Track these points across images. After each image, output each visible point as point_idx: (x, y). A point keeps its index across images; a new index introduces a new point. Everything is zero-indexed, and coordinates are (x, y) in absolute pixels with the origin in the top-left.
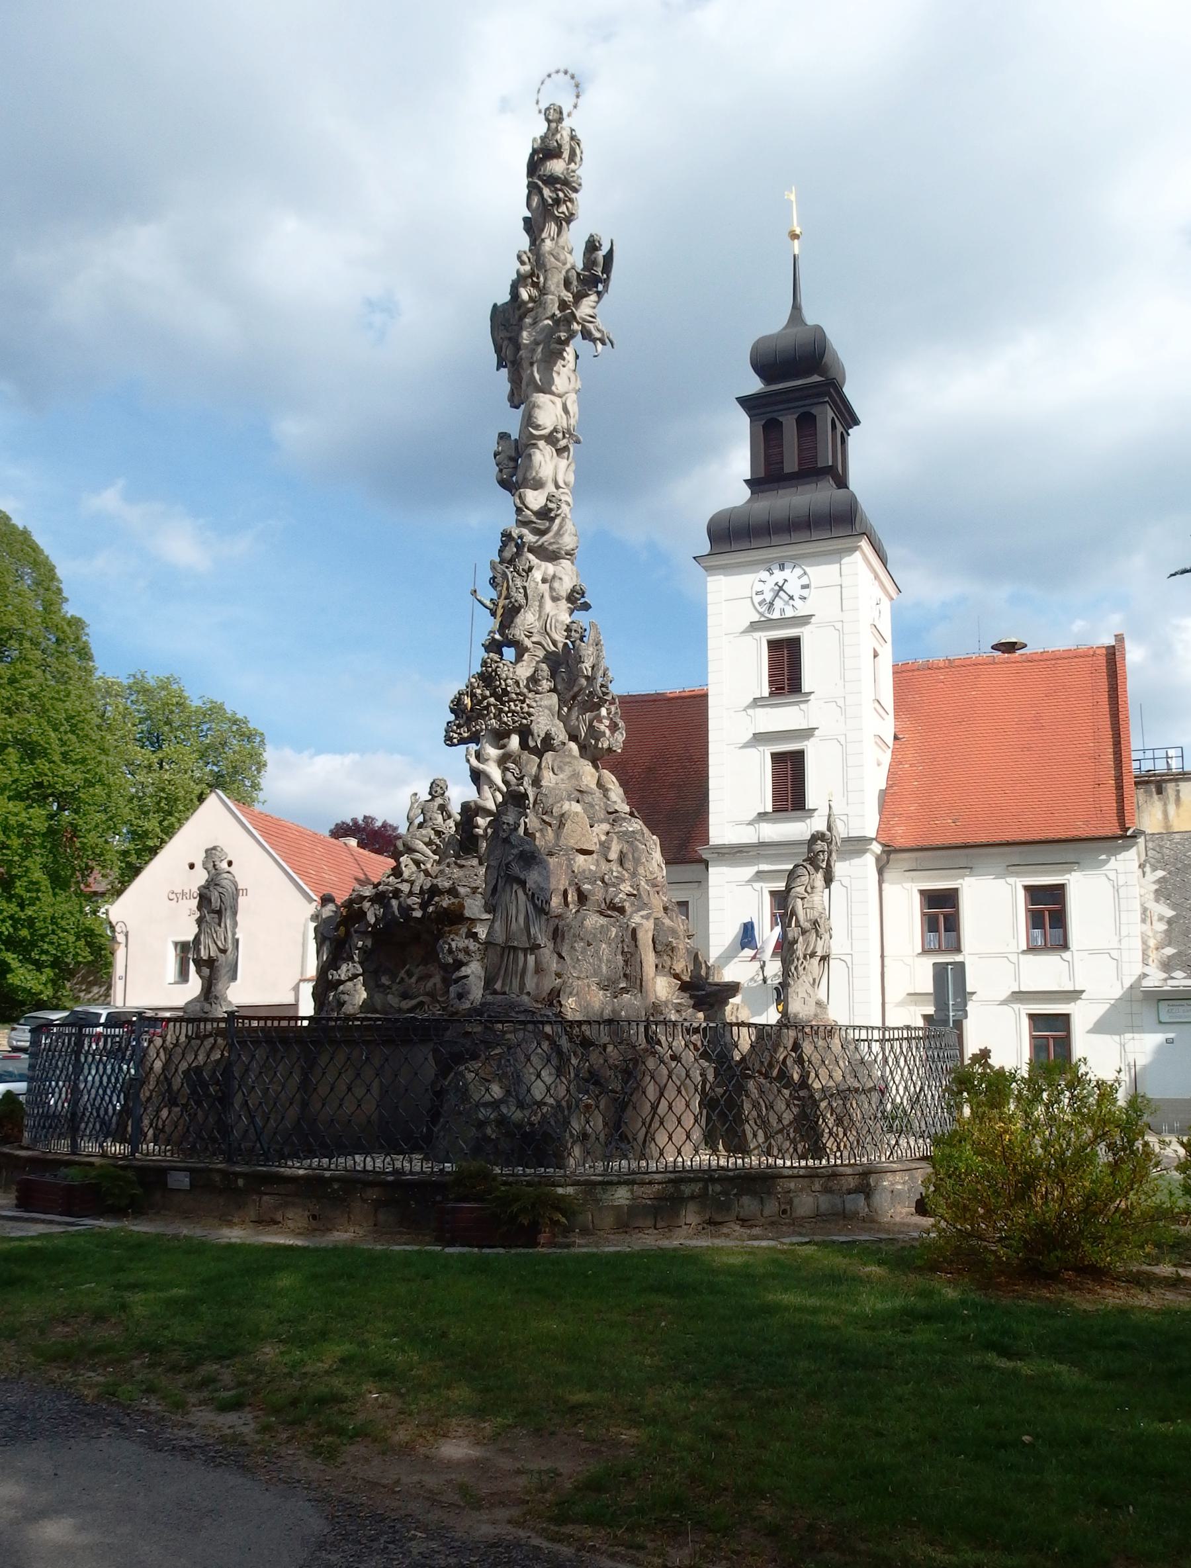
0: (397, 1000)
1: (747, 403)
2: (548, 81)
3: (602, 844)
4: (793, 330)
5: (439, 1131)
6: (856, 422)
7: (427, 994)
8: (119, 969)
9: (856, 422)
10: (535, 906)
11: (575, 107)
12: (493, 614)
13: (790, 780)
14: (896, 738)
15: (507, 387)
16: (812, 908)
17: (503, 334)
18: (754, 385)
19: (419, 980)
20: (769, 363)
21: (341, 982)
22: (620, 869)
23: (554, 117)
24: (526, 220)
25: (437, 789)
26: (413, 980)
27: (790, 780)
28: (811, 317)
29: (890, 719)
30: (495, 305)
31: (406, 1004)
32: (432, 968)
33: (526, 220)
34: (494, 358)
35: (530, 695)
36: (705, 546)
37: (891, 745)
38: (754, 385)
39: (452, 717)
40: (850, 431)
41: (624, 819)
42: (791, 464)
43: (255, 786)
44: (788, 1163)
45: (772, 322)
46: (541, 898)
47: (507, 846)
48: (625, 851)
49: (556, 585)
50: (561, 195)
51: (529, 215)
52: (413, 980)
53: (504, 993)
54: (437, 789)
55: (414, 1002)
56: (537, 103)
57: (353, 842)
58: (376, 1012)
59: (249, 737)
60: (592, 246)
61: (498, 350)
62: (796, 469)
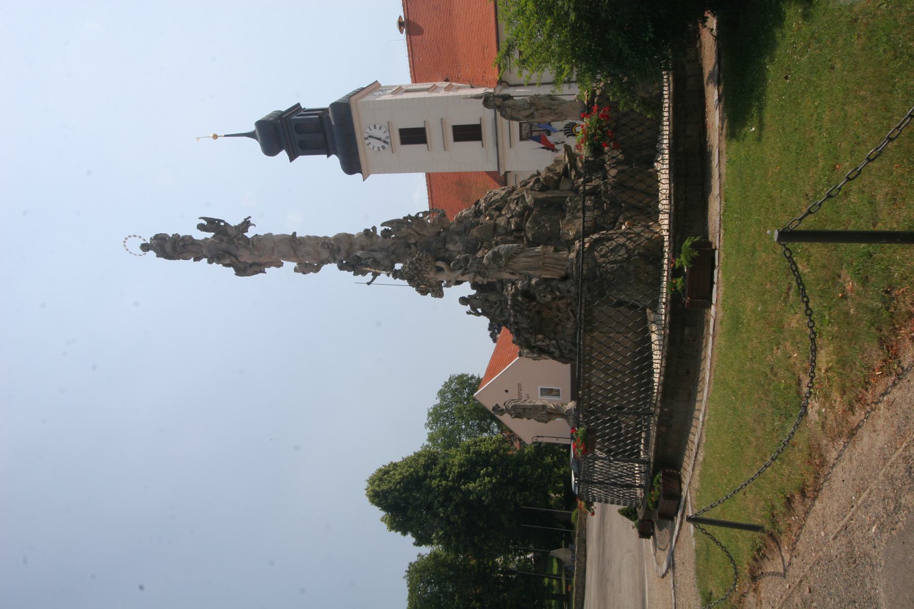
1: (292, 158)
6: (299, 104)
8: (554, 441)
9: (299, 104)
12: (379, 274)
14: (447, 80)
15: (273, 268)
18: (283, 154)
19: (559, 311)
20: (270, 150)
21: (550, 37)
23: (145, 247)
24: (195, 260)
25: (464, 301)
27: (467, 133)
31: (573, 319)
33: (195, 260)
34: (260, 274)
36: (358, 176)
38: (283, 154)
39: (429, 294)
43: (473, 377)
45: (255, 145)
54: (464, 301)
55: (571, 314)
57: (498, 336)
58: (575, 333)
59: (451, 381)
60: (201, 227)
61: (256, 273)
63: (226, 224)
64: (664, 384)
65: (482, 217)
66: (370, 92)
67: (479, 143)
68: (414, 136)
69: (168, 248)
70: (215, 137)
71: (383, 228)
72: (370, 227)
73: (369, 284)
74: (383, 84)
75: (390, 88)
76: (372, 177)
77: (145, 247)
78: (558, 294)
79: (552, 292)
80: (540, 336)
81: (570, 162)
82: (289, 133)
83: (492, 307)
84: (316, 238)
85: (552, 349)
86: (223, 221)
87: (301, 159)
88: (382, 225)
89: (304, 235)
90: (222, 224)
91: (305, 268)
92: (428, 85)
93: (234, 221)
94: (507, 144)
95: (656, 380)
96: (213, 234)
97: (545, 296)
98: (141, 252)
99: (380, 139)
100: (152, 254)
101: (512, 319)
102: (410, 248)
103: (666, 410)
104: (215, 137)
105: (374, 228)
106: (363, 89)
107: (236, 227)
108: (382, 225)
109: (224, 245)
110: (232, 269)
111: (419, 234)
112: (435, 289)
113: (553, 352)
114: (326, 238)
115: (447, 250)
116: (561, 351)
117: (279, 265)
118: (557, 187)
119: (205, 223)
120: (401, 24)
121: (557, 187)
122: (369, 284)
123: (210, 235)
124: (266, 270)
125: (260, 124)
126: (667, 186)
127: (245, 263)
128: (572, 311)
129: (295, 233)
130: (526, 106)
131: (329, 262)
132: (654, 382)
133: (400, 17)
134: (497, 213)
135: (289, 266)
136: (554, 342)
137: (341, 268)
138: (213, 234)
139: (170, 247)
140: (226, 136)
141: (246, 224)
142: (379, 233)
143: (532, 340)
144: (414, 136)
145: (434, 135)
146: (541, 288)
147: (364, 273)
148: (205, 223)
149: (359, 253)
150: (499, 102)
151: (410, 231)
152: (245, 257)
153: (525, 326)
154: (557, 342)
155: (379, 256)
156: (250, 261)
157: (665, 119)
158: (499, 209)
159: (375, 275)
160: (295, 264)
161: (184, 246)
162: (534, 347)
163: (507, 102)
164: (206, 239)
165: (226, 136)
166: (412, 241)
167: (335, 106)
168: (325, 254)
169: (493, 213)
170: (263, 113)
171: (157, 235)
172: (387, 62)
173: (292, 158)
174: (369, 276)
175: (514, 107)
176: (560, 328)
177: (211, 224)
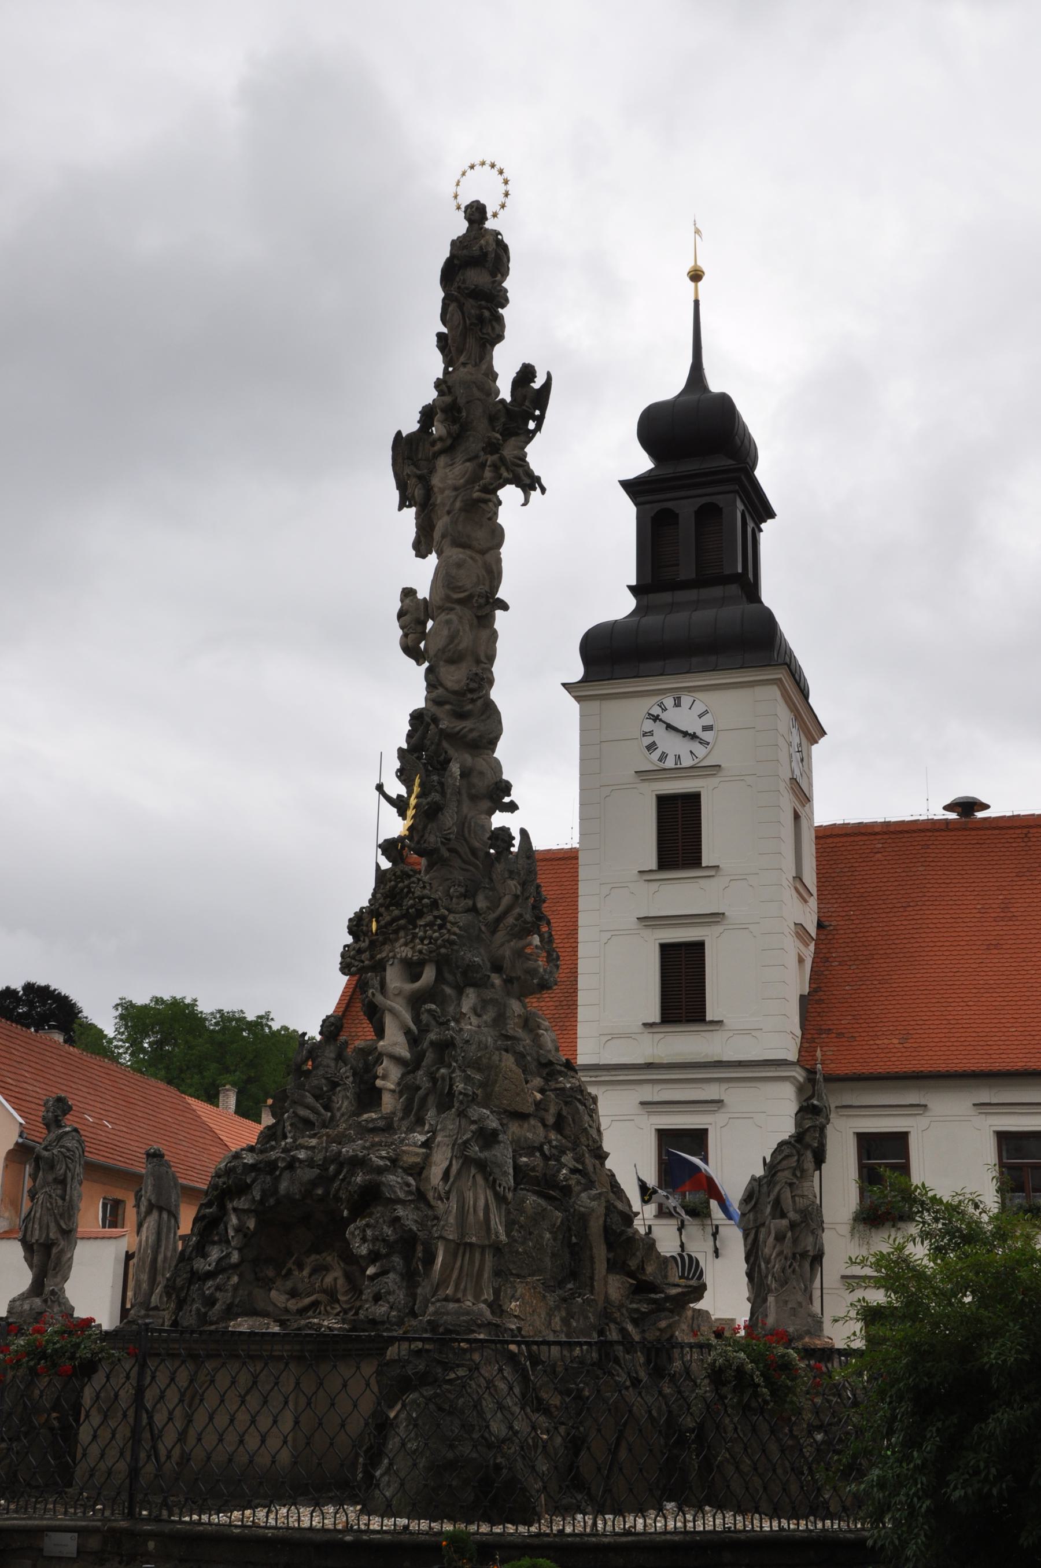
0: (283, 1298)
1: (631, 487)
2: (469, 172)
3: (537, 1104)
4: (693, 397)
5: (382, 1475)
6: (770, 514)
7: (324, 1291)
9: (770, 514)
10: (496, 1195)
11: (503, 206)
12: (402, 814)
13: (683, 984)
14: (820, 926)
16: (803, 1196)
17: (408, 470)
18: (641, 463)
20: (658, 428)
22: (559, 1137)
23: (476, 213)
24: (440, 336)
26: (306, 1273)
27: (683, 984)
28: (715, 384)
29: (813, 902)
30: (399, 433)
31: (293, 1305)
32: (329, 1258)
33: (440, 336)
34: (396, 495)
35: (451, 918)
36: (576, 671)
37: (814, 935)
38: (641, 463)
39: (349, 940)
40: (763, 526)
41: (560, 1073)
42: (687, 571)
44: (671, 1525)
45: (670, 385)
46: (504, 1184)
47: (463, 1121)
48: (564, 1113)
49: (475, 780)
50: (486, 313)
51: (445, 330)
52: (306, 1273)
53: (458, 1301)
55: (307, 1301)
56: (456, 197)
60: (527, 373)
62: (694, 576)
63: (530, 435)
64: (221, 1538)
65: (538, 1081)
66: (798, 717)
67: (655, 1016)
68: (680, 834)
69: (476, 277)
70: (696, 276)
71: (516, 834)
72: (515, 796)
73: (380, 788)
74: (817, 750)
75: (808, 774)
76: (572, 707)
77: (476, 213)
78: (370, 1271)
79: (374, 1257)
80: (251, 1224)
81: (668, 1298)
82: (699, 469)
83: (317, 1097)
84: (491, 658)
85: (215, 1254)
86: (539, 428)
87: (627, 511)
88: (524, 833)
89: (497, 626)
90: (532, 425)
91: (413, 613)
92: (810, 878)
93: (537, 455)
94: (649, 1093)
95: (473, 1528)
96: (508, 399)
97: (364, 1240)
98: (465, 201)
99: (669, 727)
100: (460, 227)
101: (302, 1155)
102: (465, 896)
103: (151, 1545)
104: (696, 276)
105: (512, 807)
106: (805, 694)
107: (523, 458)
108: (524, 833)
109: (481, 426)
110: (415, 427)
111: (499, 920)
112: (365, 956)
113: (205, 1256)
114: (491, 682)
115: (460, 991)
116: (210, 1275)
117: (421, 548)
118: (613, 1266)
119: (537, 384)
120: (967, 807)
121: (613, 1266)
122: (380, 788)
123: (505, 393)
124: (411, 512)
125: (725, 406)
126: (306, 1523)
127: (432, 471)
128: (315, 1304)
129: (505, 607)
130: (801, 1203)
131: (431, 686)
132: (469, 1522)
133: (986, 807)
134: (551, 1120)
135: (422, 574)
136: (235, 1257)
137: (417, 718)
138: (508, 399)
139: (476, 276)
140: (697, 303)
141: (530, 483)
142: (499, 820)
143: (242, 1203)
144: (680, 834)
145: (681, 895)
146: (388, 1231)
147: (403, 775)
148: (537, 384)
149: (455, 768)
150: (811, 1140)
151: (506, 901)
152: (447, 475)
153: (283, 1186)
154: (235, 1266)
155: (449, 819)
156: (436, 481)
157: (784, 1523)
158: (559, 1125)
159: (400, 805)
160: (423, 592)
161: (481, 319)
162: (222, 1208)
163: (809, 1155)
164: (494, 376)
165: (697, 303)
166: (482, 903)
167: (768, 623)
168: (454, 677)
169: (553, 1110)
170: (755, 418)
171: (505, 248)
172: (871, 775)
173: (631, 487)
174: (396, 788)
175: (800, 1173)
176: (270, 1273)
177: (532, 398)
